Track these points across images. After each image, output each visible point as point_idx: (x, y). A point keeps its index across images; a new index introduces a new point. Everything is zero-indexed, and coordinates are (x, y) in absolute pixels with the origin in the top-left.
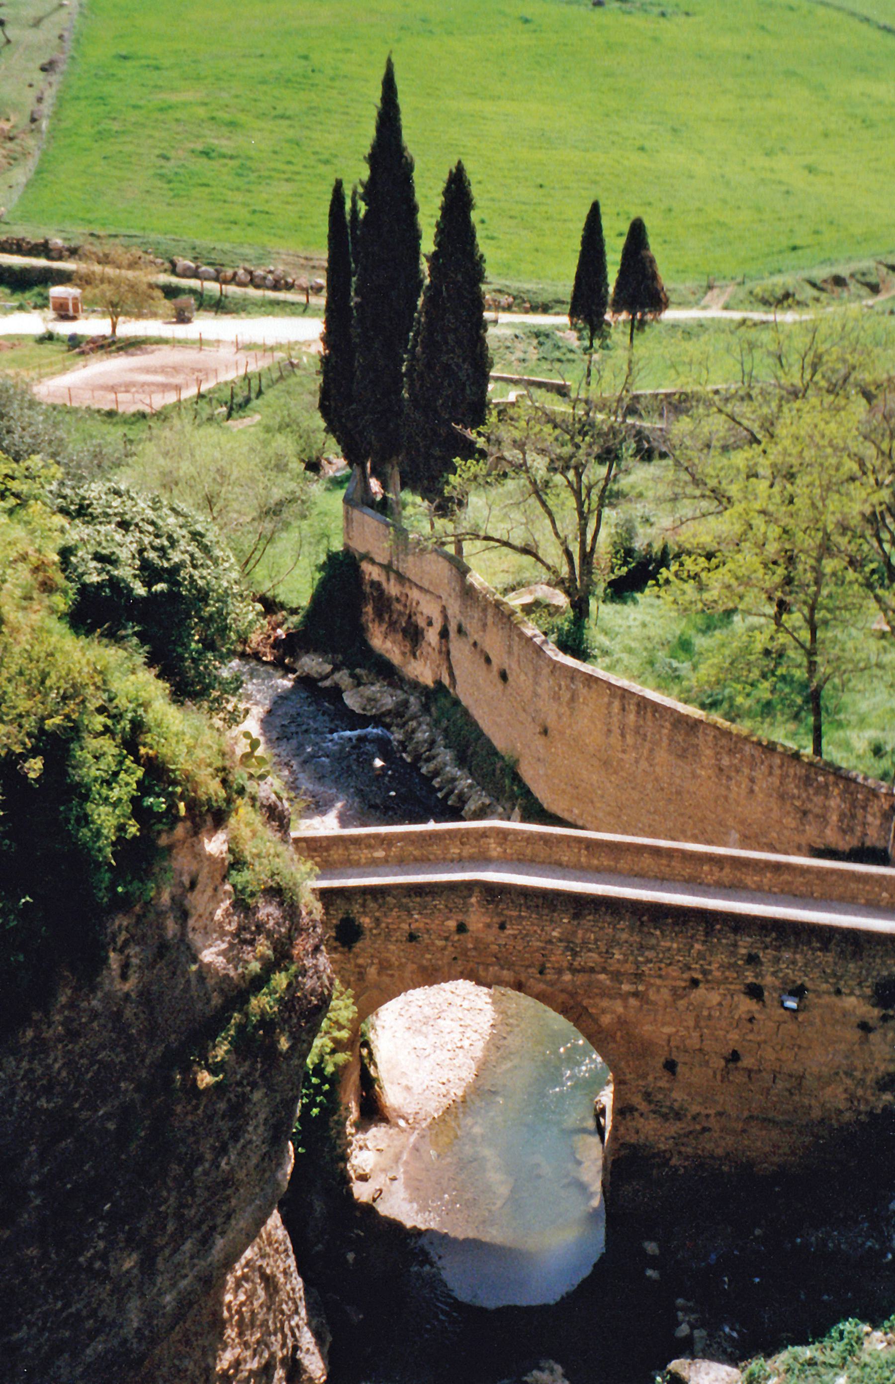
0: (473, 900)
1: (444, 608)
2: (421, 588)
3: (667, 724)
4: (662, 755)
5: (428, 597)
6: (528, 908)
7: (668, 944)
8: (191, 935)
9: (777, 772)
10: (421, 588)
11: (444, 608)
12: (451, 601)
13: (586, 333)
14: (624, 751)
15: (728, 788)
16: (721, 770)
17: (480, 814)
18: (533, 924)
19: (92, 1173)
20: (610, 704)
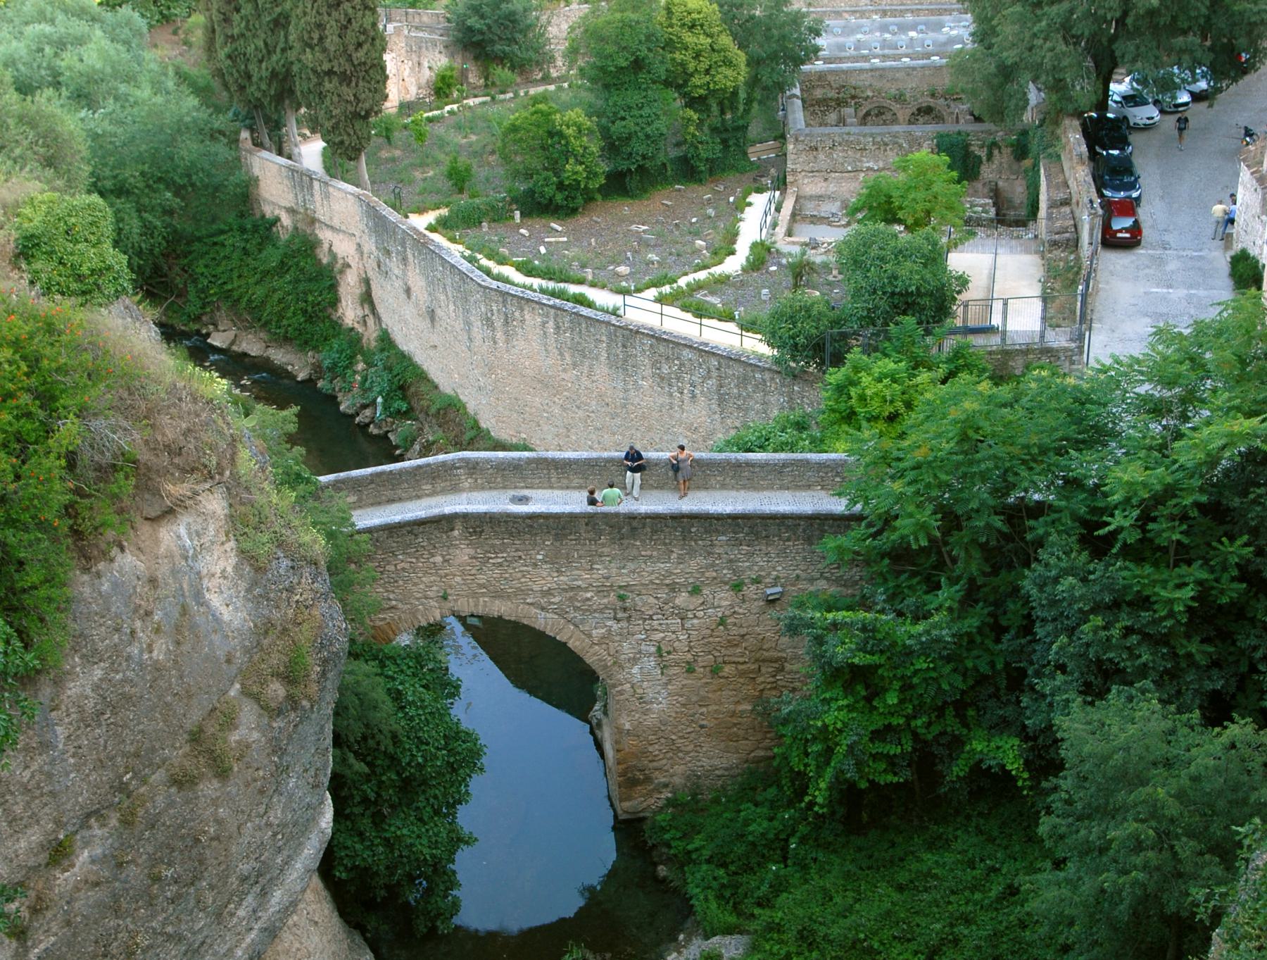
0: (456, 533)
1: (359, 245)
2: (332, 228)
3: (604, 338)
4: (602, 370)
5: (341, 236)
6: (511, 534)
7: (649, 553)
8: (207, 596)
9: (715, 374)
10: (332, 228)
11: (359, 245)
12: (366, 237)
13: (1244, 854)
14: (564, 370)
15: (671, 395)
16: (662, 379)
17: (427, 450)
18: (517, 550)
19: (1205, 69)
20: (544, 324)
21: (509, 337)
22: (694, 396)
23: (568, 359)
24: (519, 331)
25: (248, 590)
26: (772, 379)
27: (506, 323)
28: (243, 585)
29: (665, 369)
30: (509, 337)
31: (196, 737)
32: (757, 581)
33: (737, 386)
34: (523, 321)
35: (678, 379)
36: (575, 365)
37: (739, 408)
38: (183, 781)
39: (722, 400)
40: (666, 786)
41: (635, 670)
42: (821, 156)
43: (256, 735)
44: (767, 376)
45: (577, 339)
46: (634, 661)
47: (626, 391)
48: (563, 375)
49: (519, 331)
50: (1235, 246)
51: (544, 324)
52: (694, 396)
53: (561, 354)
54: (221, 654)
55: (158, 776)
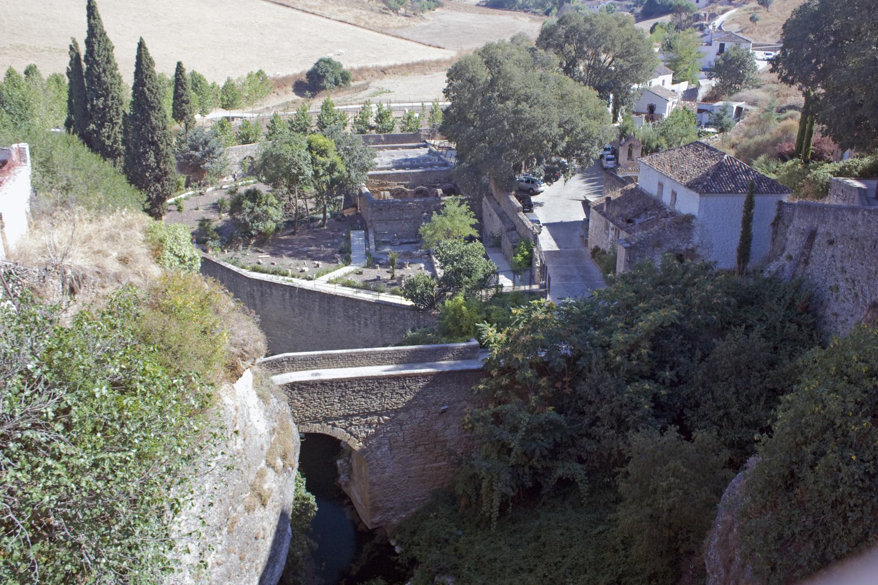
15: (354, 325)
20: (283, 295)
21: (263, 303)
22: (366, 325)
23: (297, 311)
24: (269, 299)
25: (264, 414)
26: (408, 313)
27: (262, 295)
28: (262, 412)
29: (351, 313)
30: (263, 303)
31: (253, 488)
32: (435, 404)
33: (390, 318)
34: (271, 294)
35: (358, 317)
36: (300, 314)
37: (391, 328)
38: (249, 509)
39: (382, 326)
40: (392, 508)
41: (378, 453)
42: (384, 213)
43: (274, 485)
44: (406, 312)
45: (302, 301)
46: (378, 448)
47: (329, 325)
48: (294, 319)
49: (269, 299)
50: (589, 245)
51: (283, 295)
52: (366, 325)
53: (293, 309)
54: (259, 445)
55: (240, 508)
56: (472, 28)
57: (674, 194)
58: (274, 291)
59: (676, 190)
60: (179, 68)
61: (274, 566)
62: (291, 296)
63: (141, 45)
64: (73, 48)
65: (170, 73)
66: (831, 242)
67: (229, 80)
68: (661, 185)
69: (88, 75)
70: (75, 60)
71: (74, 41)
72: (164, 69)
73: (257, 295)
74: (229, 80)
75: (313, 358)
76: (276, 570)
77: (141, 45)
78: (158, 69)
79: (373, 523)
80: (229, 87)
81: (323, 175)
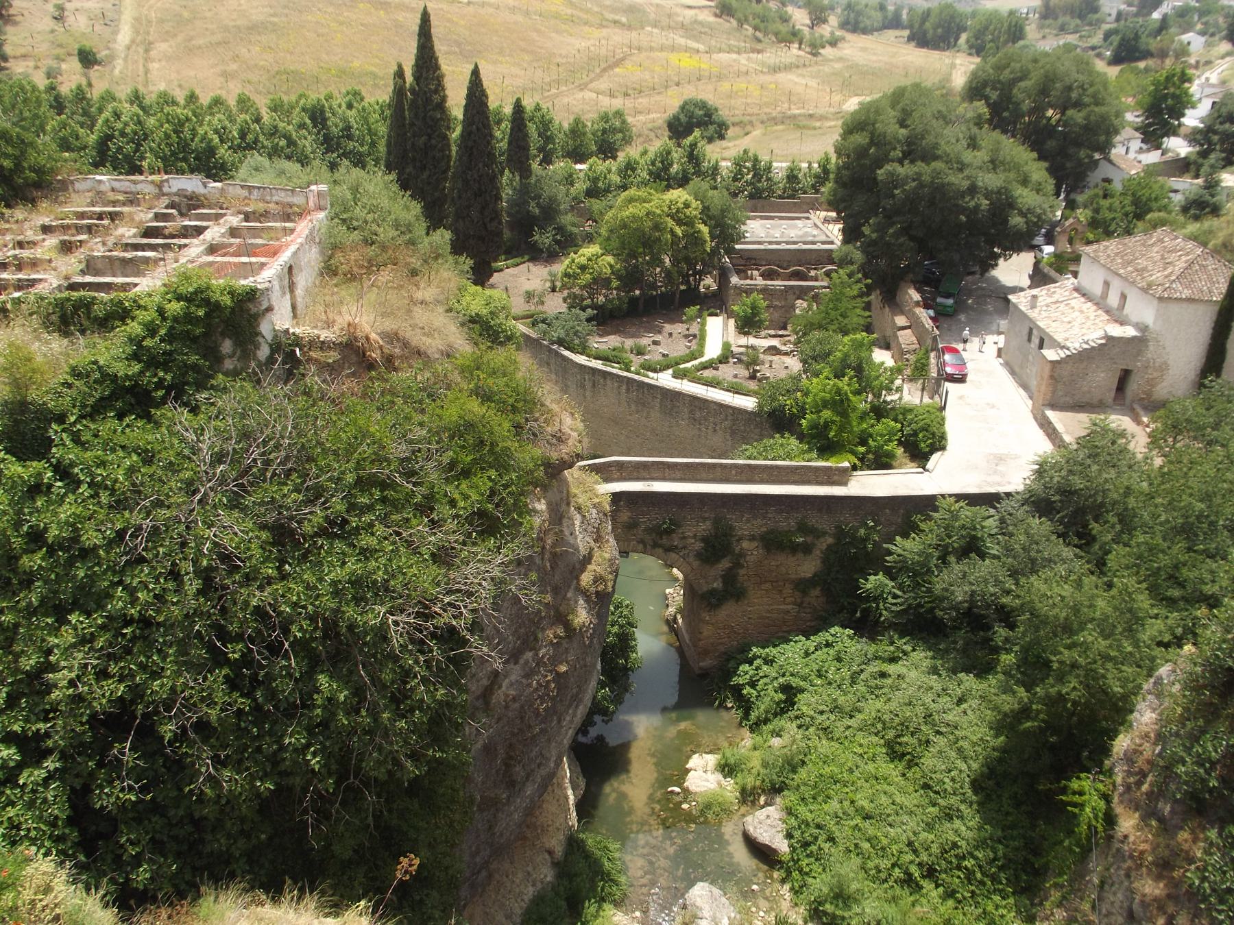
20: (619, 387)
29: (698, 415)
36: (637, 412)
51: (619, 387)
56: (888, 62)
57: (1124, 297)
58: (609, 382)
59: (1126, 292)
60: (518, 108)
61: (577, 707)
62: (628, 390)
63: (476, 72)
64: (400, 74)
65: (508, 110)
66: (839, 660)
67: (578, 121)
68: (1107, 284)
69: (419, 96)
70: (399, 92)
71: (400, 66)
72: (499, 100)
73: (588, 384)
74: (578, 121)
75: (645, 465)
76: (579, 712)
77: (476, 72)
78: (493, 104)
79: (701, 668)
80: (576, 131)
81: (168, 677)
